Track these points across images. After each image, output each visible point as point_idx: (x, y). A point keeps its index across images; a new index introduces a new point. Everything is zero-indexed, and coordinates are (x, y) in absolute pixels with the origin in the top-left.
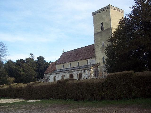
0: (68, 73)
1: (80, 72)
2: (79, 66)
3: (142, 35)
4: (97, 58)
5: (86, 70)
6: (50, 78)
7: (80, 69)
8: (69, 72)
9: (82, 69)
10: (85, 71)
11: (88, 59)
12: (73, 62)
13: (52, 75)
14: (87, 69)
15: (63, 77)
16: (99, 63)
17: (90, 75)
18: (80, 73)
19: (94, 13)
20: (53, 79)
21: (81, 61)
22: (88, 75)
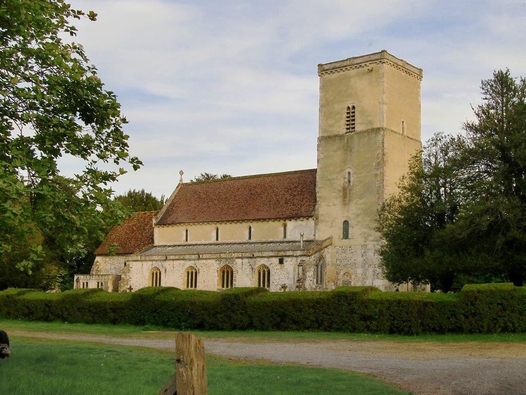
0: (213, 261)
1: (263, 261)
2: (253, 240)
3: (81, 220)
4: (323, 221)
5: (285, 259)
6: (131, 275)
7: (265, 254)
8: (219, 259)
9: (271, 254)
10: (281, 262)
11: (290, 218)
12: (228, 225)
13: (145, 263)
14: (289, 256)
15: (192, 276)
16: (330, 238)
17: (304, 274)
18: (264, 266)
19: (326, 67)
20: (147, 277)
21: (260, 224)
22: (291, 276)
